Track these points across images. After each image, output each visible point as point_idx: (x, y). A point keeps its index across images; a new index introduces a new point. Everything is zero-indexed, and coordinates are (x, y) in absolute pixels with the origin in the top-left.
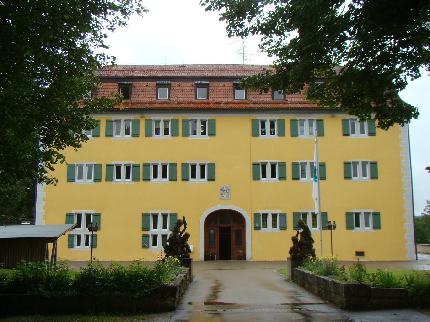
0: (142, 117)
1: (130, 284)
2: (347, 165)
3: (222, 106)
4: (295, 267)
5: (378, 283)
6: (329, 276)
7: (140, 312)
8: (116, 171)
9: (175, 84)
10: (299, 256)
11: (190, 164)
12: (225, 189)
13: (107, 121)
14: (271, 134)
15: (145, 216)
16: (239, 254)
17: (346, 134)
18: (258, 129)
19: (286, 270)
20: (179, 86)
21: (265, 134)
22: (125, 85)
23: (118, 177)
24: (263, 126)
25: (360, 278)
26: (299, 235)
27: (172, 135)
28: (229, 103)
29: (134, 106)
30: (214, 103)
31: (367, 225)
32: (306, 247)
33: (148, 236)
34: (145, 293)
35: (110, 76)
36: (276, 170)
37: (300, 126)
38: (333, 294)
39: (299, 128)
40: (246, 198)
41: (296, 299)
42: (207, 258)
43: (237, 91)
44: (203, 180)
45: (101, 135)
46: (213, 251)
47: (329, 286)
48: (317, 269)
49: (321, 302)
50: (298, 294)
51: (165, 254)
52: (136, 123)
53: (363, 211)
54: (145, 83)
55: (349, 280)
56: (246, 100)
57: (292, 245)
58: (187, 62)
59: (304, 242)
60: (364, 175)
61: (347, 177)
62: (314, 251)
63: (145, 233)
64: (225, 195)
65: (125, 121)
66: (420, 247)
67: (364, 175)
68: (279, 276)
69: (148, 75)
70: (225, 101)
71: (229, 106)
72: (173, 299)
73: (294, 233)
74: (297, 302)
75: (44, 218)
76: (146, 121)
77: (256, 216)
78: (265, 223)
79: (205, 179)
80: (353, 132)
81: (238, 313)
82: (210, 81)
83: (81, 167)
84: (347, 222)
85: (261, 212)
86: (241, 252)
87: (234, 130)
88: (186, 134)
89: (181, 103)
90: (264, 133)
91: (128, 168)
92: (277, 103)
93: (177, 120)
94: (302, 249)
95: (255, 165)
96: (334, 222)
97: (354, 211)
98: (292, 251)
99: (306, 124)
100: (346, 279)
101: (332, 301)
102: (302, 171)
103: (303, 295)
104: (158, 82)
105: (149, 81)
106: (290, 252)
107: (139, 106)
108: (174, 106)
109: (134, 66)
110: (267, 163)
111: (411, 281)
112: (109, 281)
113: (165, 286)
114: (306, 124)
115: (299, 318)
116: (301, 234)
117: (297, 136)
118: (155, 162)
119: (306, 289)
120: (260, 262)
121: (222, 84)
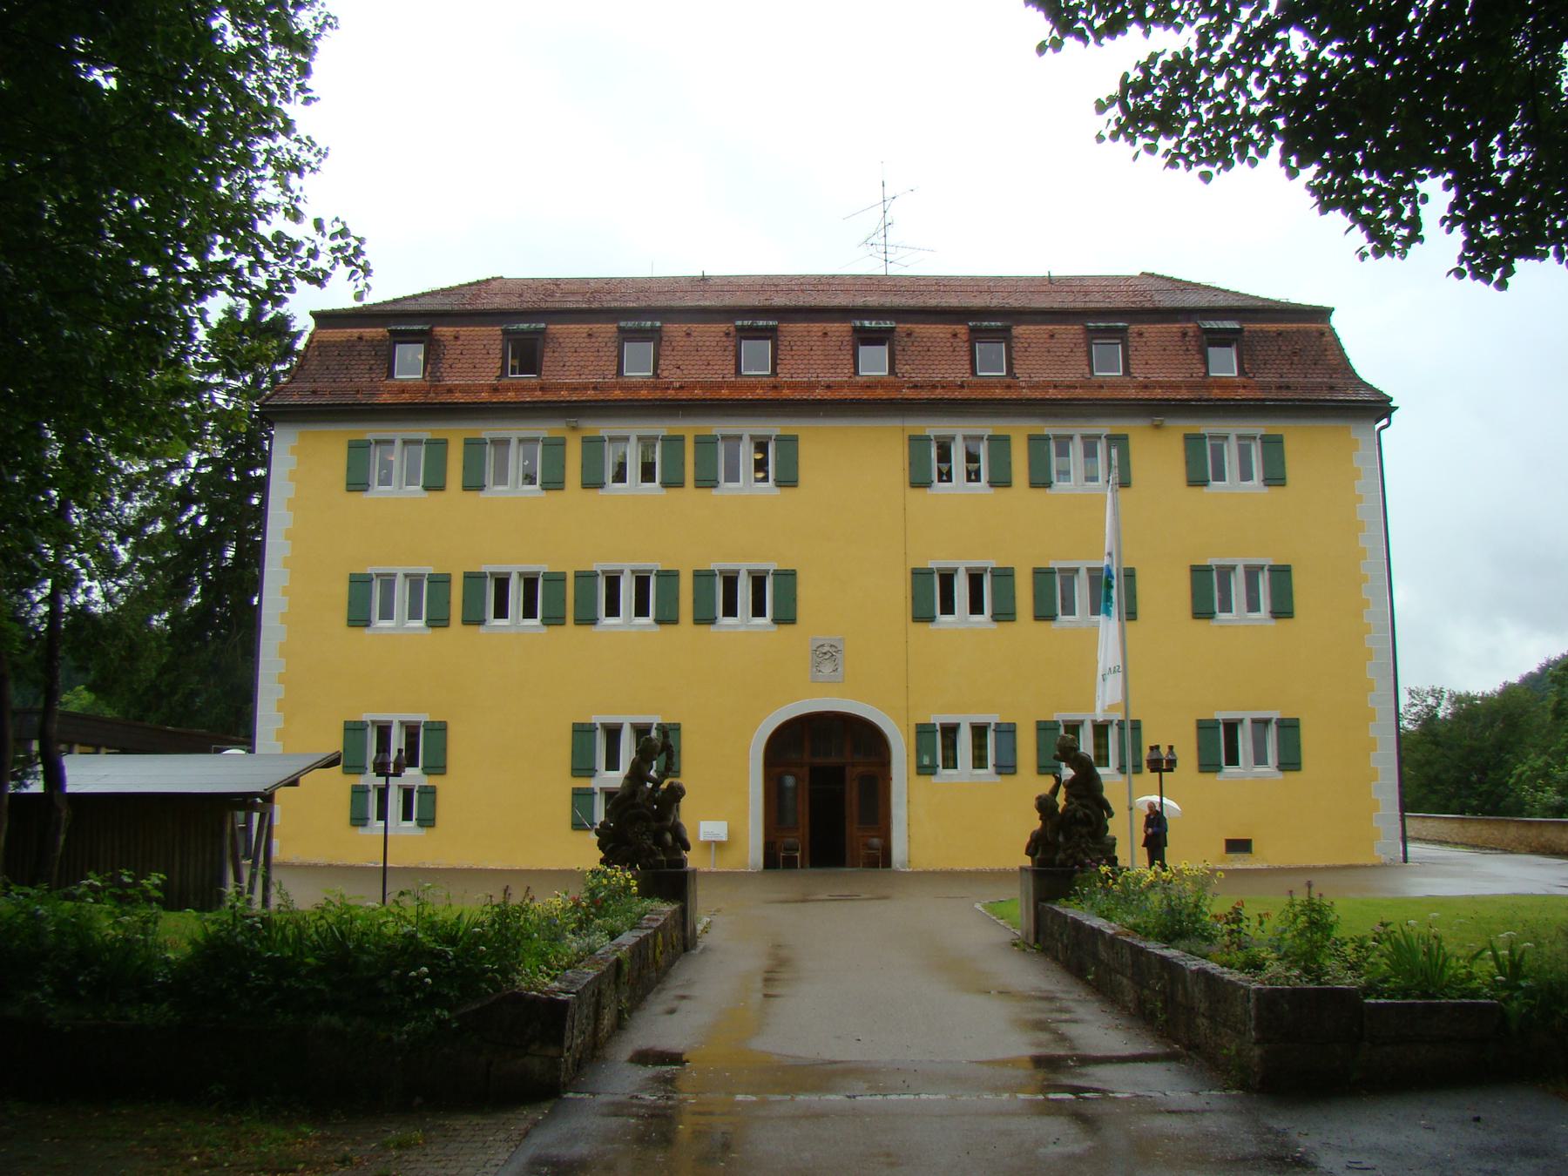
0: (574, 429)
1: (382, 984)
2: (1200, 573)
3: (819, 394)
4: (1045, 900)
5: (1385, 980)
6: (1183, 943)
7: (418, 1100)
8: (490, 595)
9: (674, 330)
10: (1062, 864)
11: (721, 572)
12: (826, 649)
13: (468, 443)
14: (969, 480)
15: (582, 732)
16: (871, 848)
17: (1197, 480)
18: (929, 464)
19: (1017, 906)
20: (688, 335)
21: (950, 480)
22: (523, 332)
23: (501, 612)
24: (945, 456)
25: (1313, 958)
26: (1062, 790)
27: (665, 485)
28: (840, 386)
29: (549, 397)
30: (793, 386)
31: (1260, 759)
32: (1084, 830)
33: (590, 793)
34: (440, 1023)
35: (480, 307)
36: (987, 591)
37: (1058, 455)
38: (1202, 1022)
39: (1054, 462)
40: (892, 679)
41: (1055, 1032)
42: (775, 858)
43: (864, 351)
44: (759, 621)
45: (448, 486)
46: (791, 840)
47: (1185, 989)
48: (1132, 914)
49: (1151, 1048)
50: (1061, 1010)
51: (601, 855)
52: (555, 447)
53: (1247, 716)
54: (584, 328)
55: (1274, 968)
56: (892, 378)
57: (1037, 824)
58: (714, 270)
59: (1080, 814)
60: (1253, 606)
61: (1202, 611)
62: (1112, 844)
63: (582, 783)
64: (827, 669)
65: (521, 441)
66: (1414, 826)
67: (1253, 606)
68: (989, 927)
69: (595, 305)
70: (827, 378)
71: (838, 395)
72: (552, 1051)
73: (1047, 784)
74: (1061, 1051)
75: (281, 735)
76: (586, 441)
77: (924, 731)
78: (950, 753)
79: (767, 620)
80: (1219, 476)
81: (817, 1116)
82: (781, 320)
83: (388, 582)
84: (1199, 749)
85: (938, 719)
86: (876, 841)
87: (854, 466)
88: (707, 481)
89: (693, 386)
90: (945, 476)
91: (530, 583)
92: (987, 384)
93: (681, 439)
94: (1070, 838)
95: (920, 576)
96: (1171, 748)
97: (1221, 715)
98: (1036, 845)
99: (1076, 449)
100: (1256, 965)
101: (1197, 1047)
102: (1063, 599)
103: (1081, 1011)
104: (622, 324)
105: (598, 322)
106: (1031, 850)
107: (564, 395)
108: (671, 394)
109: (556, 282)
110: (956, 570)
111: (1514, 968)
112: (304, 972)
113: (519, 998)
114: (1076, 449)
115: (1077, 1148)
116: (1070, 785)
117: (1048, 485)
118: (612, 566)
119: (1088, 983)
120: (934, 873)
121: (817, 327)
